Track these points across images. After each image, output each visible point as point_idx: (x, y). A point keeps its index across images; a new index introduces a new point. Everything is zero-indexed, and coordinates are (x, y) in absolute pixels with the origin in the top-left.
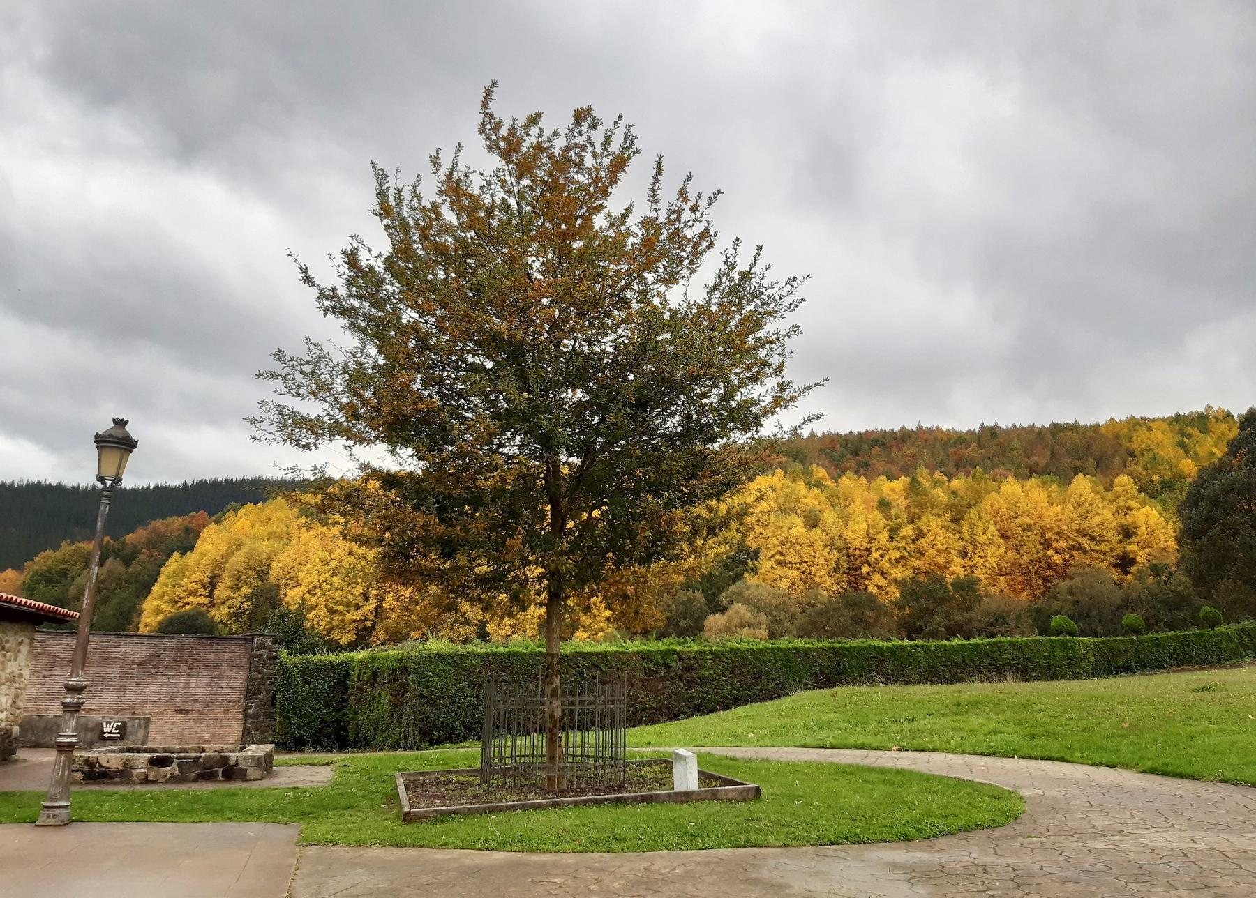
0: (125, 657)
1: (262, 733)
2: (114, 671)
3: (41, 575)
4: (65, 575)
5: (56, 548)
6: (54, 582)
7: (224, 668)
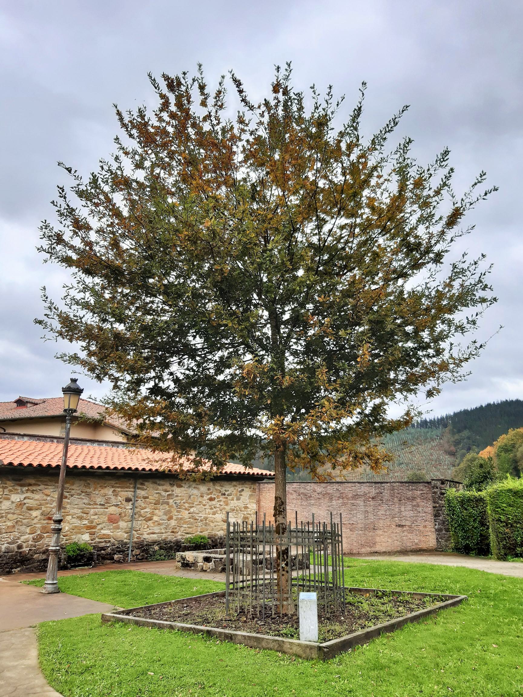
0: (365, 495)
1: (446, 541)
2: (360, 502)
3: (502, 448)
4: (514, 447)
5: (507, 433)
6: (509, 451)
7: (419, 500)
